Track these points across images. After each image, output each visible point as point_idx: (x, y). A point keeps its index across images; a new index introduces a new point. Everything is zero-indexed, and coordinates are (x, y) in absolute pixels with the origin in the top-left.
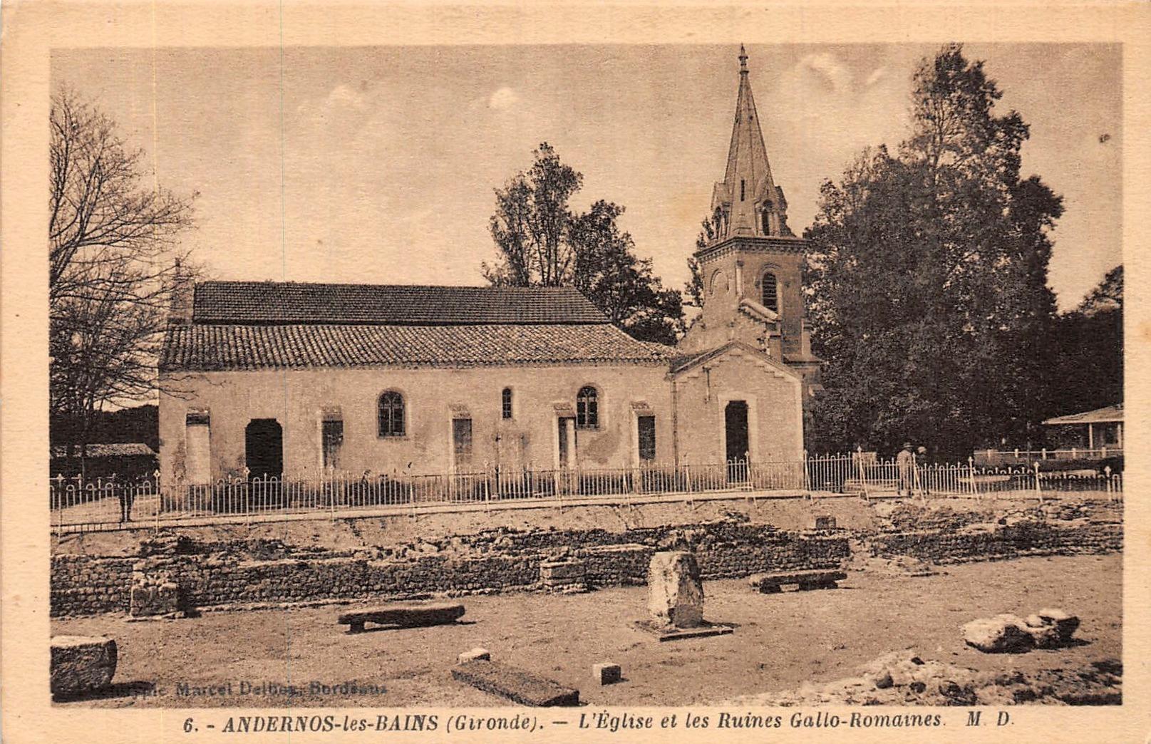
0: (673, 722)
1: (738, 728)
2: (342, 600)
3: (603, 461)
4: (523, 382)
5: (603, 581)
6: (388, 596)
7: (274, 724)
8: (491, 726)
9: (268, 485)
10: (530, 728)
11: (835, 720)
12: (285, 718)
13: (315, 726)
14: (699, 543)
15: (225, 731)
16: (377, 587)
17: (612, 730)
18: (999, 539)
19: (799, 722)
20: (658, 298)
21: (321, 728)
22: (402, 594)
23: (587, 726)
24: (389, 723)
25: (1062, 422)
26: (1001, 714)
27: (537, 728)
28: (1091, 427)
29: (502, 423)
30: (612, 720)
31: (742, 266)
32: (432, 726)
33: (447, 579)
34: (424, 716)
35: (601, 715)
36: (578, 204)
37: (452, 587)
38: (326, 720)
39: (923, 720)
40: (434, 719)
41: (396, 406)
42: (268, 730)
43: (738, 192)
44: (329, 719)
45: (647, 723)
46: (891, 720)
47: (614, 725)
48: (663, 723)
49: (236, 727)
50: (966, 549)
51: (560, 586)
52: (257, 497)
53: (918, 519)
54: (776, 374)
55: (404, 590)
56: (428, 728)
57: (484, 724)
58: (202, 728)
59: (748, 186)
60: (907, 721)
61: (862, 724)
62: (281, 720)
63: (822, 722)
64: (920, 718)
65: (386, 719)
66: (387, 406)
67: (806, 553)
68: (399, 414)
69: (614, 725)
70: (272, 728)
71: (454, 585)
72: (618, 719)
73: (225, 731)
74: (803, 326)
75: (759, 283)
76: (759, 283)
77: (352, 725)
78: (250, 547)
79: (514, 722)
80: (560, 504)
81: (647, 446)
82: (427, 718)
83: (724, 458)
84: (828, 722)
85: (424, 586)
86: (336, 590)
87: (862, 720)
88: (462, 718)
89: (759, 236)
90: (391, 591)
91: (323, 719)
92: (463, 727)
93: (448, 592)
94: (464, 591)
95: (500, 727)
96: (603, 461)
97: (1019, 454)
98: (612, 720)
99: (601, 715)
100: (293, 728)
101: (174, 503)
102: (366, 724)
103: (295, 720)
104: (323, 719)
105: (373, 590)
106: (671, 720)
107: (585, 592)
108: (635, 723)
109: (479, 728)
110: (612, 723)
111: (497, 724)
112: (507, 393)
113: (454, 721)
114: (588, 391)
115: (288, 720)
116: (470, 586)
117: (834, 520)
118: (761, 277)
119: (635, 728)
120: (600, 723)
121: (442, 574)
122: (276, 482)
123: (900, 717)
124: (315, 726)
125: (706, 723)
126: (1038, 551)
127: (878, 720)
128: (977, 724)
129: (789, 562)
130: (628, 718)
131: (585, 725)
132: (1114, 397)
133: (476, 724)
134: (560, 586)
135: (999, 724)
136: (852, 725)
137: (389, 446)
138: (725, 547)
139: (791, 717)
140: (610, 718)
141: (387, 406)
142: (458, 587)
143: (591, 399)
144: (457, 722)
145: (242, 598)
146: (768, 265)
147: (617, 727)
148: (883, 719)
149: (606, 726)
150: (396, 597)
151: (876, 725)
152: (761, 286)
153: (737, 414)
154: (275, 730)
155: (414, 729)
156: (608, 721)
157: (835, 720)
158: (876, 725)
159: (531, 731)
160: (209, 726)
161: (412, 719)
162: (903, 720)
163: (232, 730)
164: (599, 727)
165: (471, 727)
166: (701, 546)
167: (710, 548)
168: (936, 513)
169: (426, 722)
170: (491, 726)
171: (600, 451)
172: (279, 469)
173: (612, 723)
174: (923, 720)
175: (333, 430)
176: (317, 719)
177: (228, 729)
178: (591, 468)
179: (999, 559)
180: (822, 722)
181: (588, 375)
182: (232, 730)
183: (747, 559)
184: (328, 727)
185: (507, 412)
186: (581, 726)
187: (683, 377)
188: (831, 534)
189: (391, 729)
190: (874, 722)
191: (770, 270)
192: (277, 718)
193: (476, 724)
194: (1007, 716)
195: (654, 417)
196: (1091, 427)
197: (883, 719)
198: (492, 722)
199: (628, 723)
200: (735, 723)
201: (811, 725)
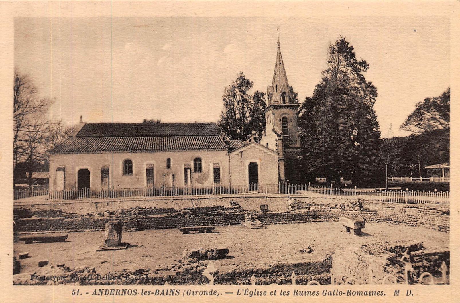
0: (275, 293)
1: (301, 296)
2: (53, 232)
3: (202, 184)
4: (174, 156)
5: (148, 227)
6: (69, 231)
7: (113, 292)
8: (201, 294)
9: (86, 191)
10: (217, 295)
11: (341, 292)
12: (117, 290)
13: (130, 293)
14: (186, 214)
15: (93, 295)
16: (66, 227)
17: (250, 296)
18: (305, 215)
19: (326, 293)
20: (235, 128)
21: (132, 294)
22: (74, 230)
23: (240, 295)
24: (160, 293)
25: (432, 167)
26: (408, 290)
27: (220, 294)
28: (443, 169)
29: (166, 170)
30: (250, 292)
31: (274, 114)
32: (177, 294)
33: (91, 226)
34: (174, 290)
35: (246, 290)
36: (353, 51)
37: (92, 228)
38: (134, 291)
39: (376, 293)
40: (178, 291)
41: (130, 165)
42: (111, 294)
43: (275, 89)
44: (135, 291)
45: (264, 293)
46: (363, 293)
47: (251, 294)
48: (271, 293)
49: (97, 293)
50: (291, 218)
51: (127, 229)
52: (83, 194)
53: (301, 206)
54: (268, 153)
55: (76, 229)
56: (176, 294)
57: (198, 293)
58: (84, 295)
59: (278, 87)
60: (370, 294)
61: (351, 294)
62: (116, 291)
63: (335, 293)
64: (375, 292)
65: (159, 291)
66: (127, 164)
67: (227, 219)
68: (131, 167)
69: (251, 294)
70: (112, 294)
71: (93, 227)
72: (253, 292)
73: (93, 295)
74: (297, 135)
75: (280, 120)
76: (280, 120)
77: (145, 293)
78: (47, 212)
79: (211, 292)
80: (221, 197)
81: (217, 178)
82: (175, 291)
83: (248, 182)
84: (338, 293)
85: (83, 227)
86: (51, 228)
87: (351, 293)
88: (190, 291)
89: (281, 104)
90: (71, 229)
91: (133, 290)
92: (190, 294)
93: (91, 229)
94: (97, 230)
95: (204, 294)
96: (202, 184)
97: (413, 179)
98: (250, 292)
99: (246, 290)
100: (121, 294)
101: (53, 196)
102: (150, 293)
103: (121, 291)
104: (133, 290)
105: (64, 228)
106: (274, 292)
107: (136, 231)
108: (259, 293)
109: (196, 294)
110: (250, 293)
111: (203, 293)
112: (169, 160)
113: (186, 291)
114: (198, 160)
115: (118, 291)
116: (99, 228)
117: (267, 206)
118: (282, 118)
119: (259, 295)
120: (245, 293)
121: (89, 224)
122: (84, 190)
123: (367, 292)
124: (130, 293)
125: (289, 294)
126: (320, 220)
127: (358, 293)
128: (398, 295)
129: (221, 221)
130: (256, 291)
131: (239, 294)
132: (447, 159)
133: (195, 293)
134: (127, 229)
135: (407, 295)
136: (348, 295)
137: (127, 179)
138: (196, 216)
139: (322, 292)
140: (249, 291)
141: (127, 164)
142: (95, 228)
143: (199, 162)
144: (187, 292)
145: (19, 230)
146: (283, 114)
147: (252, 294)
148: (360, 293)
149: (248, 294)
150: (72, 231)
151: (357, 295)
152: (281, 121)
153: (253, 169)
154: (113, 295)
155: (170, 295)
156: (249, 293)
157: (341, 292)
158: (357, 295)
159: (217, 296)
160: (88, 293)
161: (169, 291)
162: (368, 293)
163: (96, 294)
164: (245, 294)
165: (193, 294)
166: (186, 216)
167: (190, 216)
168: (308, 204)
169: (175, 292)
170: (201, 294)
171: (201, 180)
172: (88, 186)
173: (250, 293)
174: (376, 293)
175: (105, 172)
176: (130, 291)
177: (94, 294)
178: (198, 185)
179: (302, 222)
180: (335, 293)
181: (197, 154)
182: (96, 294)
183: (204, 220)
184: (135, 294)
185: (169, 166)
186: (238, 294)
187: (233, 154)
188: (239, 212)
189: (161, 295)
190: (356, 294)
191: (285, 116)
192: (114, 290)
193: (195, 293)
194: (411, 291)
195: (219, 168)
196: (443, 169)
197: (360, 293)
198: (201, 292)
199: (256, 293)
200: (300, 294)
201: (331, 295)
